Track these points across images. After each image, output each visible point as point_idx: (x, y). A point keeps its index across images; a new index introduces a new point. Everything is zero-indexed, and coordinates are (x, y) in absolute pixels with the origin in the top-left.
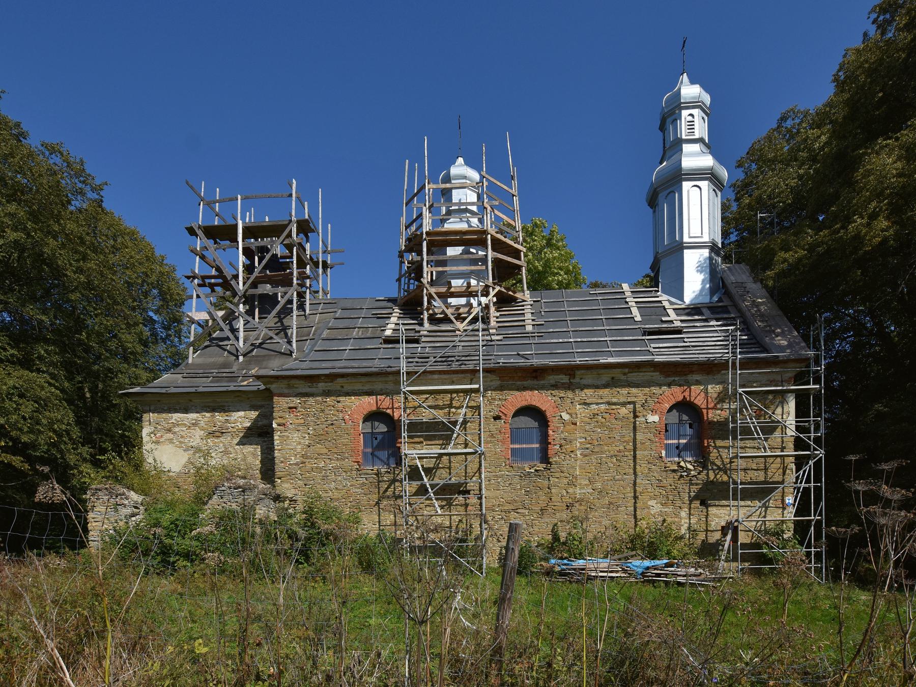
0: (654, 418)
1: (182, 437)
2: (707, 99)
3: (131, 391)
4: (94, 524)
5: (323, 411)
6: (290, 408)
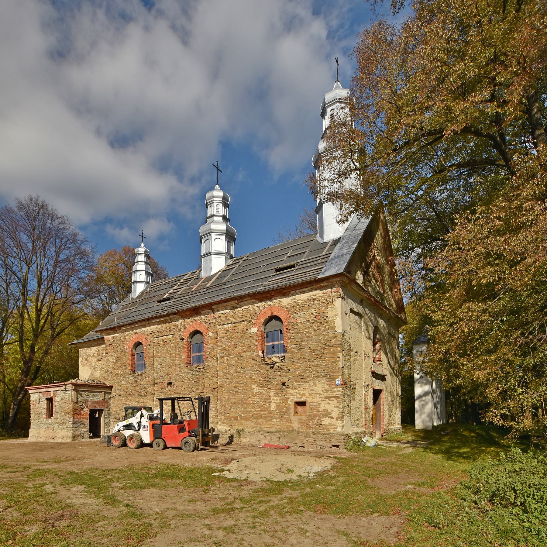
0: (254, 330)
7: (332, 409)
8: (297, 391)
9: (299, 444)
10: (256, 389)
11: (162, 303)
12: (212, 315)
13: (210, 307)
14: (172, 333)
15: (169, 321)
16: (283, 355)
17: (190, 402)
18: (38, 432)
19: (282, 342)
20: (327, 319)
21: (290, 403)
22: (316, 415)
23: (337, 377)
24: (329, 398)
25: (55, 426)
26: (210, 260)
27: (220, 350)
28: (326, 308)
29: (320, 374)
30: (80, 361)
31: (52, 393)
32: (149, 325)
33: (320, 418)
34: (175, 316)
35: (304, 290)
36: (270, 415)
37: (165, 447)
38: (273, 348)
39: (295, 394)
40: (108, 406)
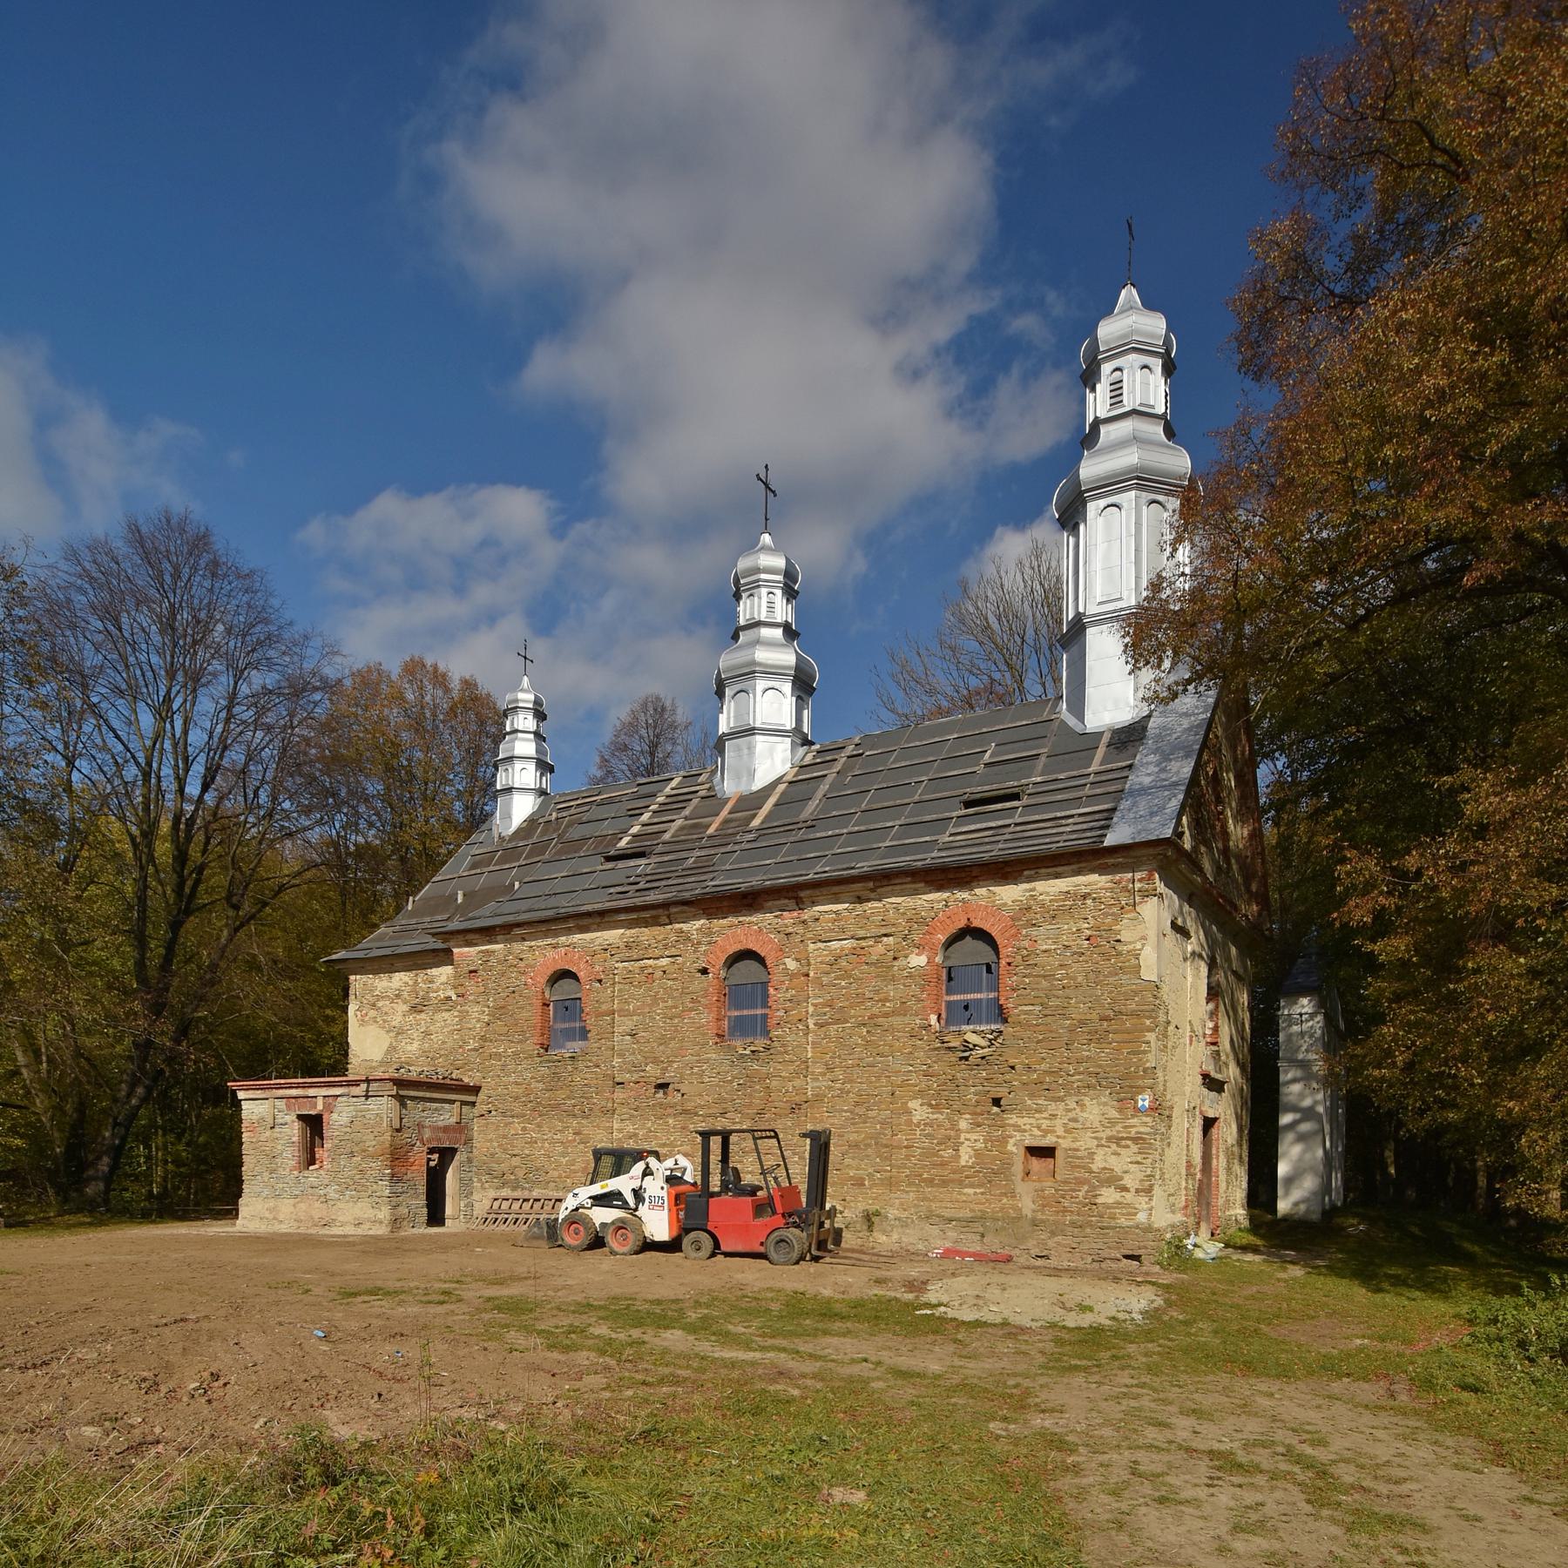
0: (918, 960)
3: (334, 957)
7: (1125, 1168)
8: (1032, 1121)
9: (1034, 1252)
10: (919, 1111)
11: (621, 864)
12: (795, 914)
13: (794, 894)
14: (674, 951)
15: (664, 919)
16: (993, 1027)
17: (774, 1141)
18: (270, 1203)
19: (992, 995)
20: (1120, 947)
21: (1014, 1149)
22: (1081, 1182)
23: (1141, 1090)
24: (1118, 1140)
25: (332, 1192)
26: (751, 748)
27: (815, 1005)
28: (1117, 919)
29: (1096, 1081)
30: (352, 1008)
31: (320, 1102)
32: (601, 927)
33: (1094, 1188)
34: (685, 908)
35: (1059, 869)
36: (957, 1176)
37: (716, 1249)
38: (966, 1008)
39: (1026, 1128)
40: (469, 1141)
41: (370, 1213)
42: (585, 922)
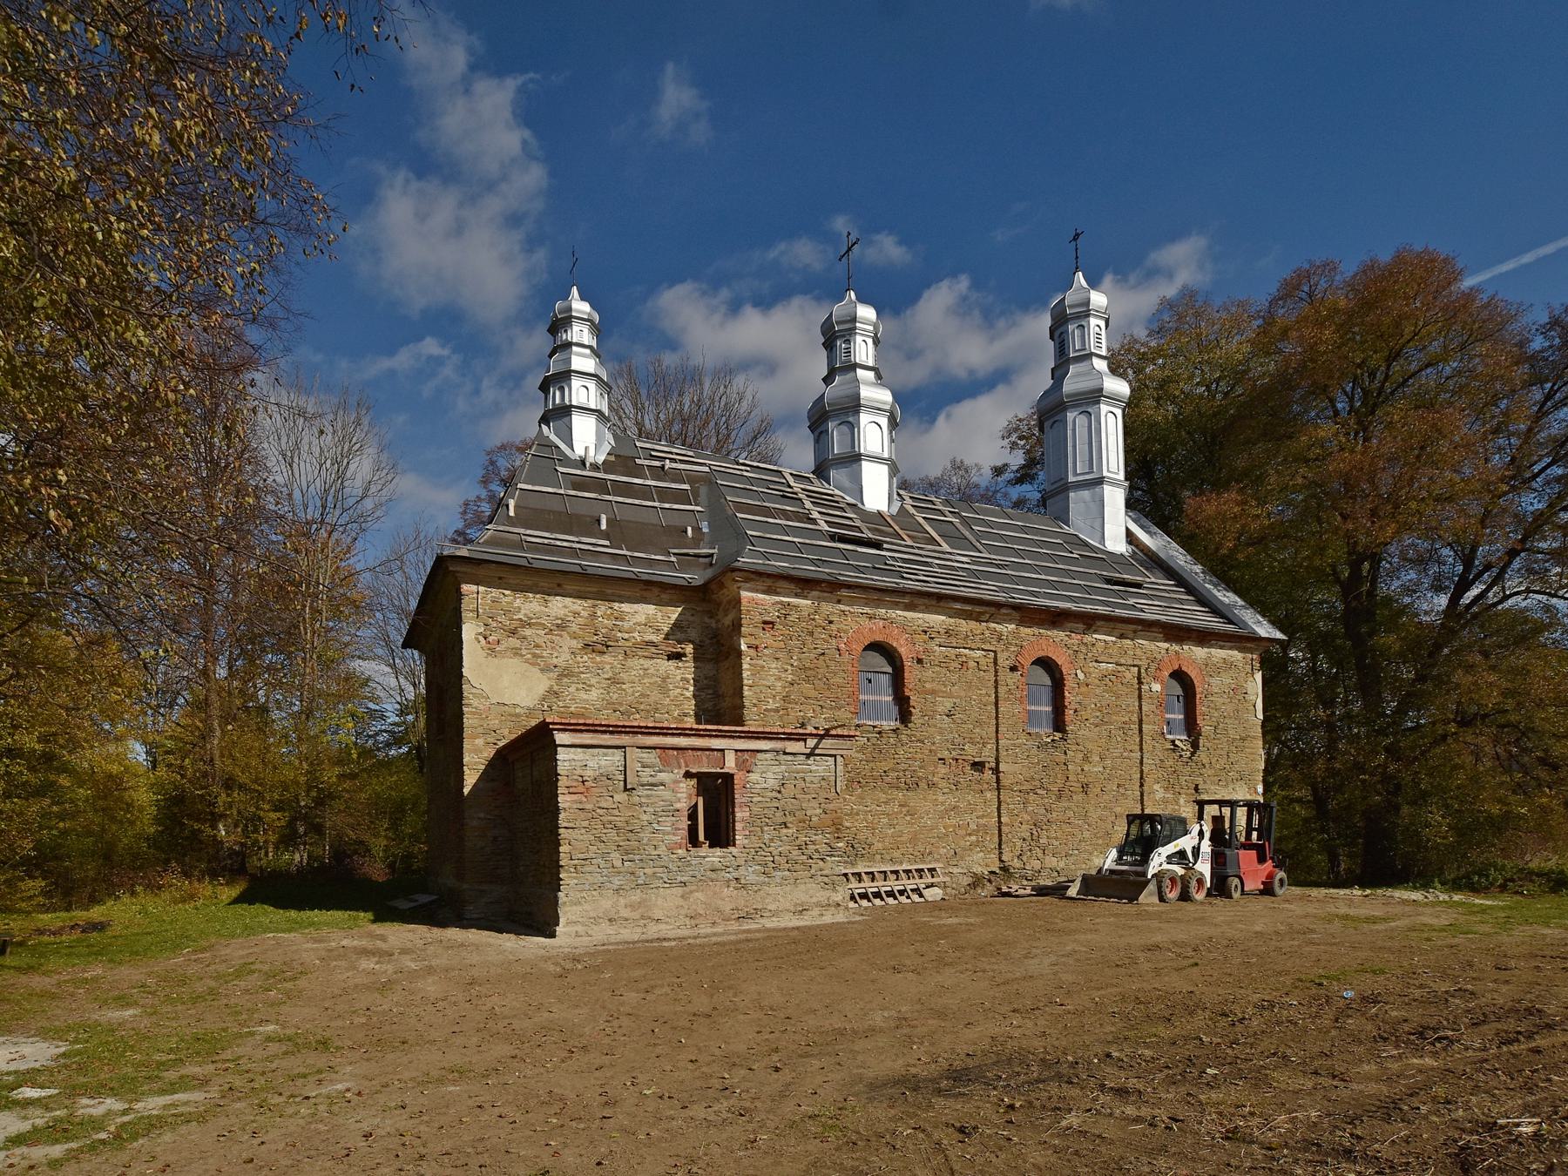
1: (537, 646)
2: (597, 318)
4: (569, 798)
5: (811, 634)
6: (765, 623)
13: (1089, 622)
30: (469, 631)
41: (822, 895)
42: (917, 601)
